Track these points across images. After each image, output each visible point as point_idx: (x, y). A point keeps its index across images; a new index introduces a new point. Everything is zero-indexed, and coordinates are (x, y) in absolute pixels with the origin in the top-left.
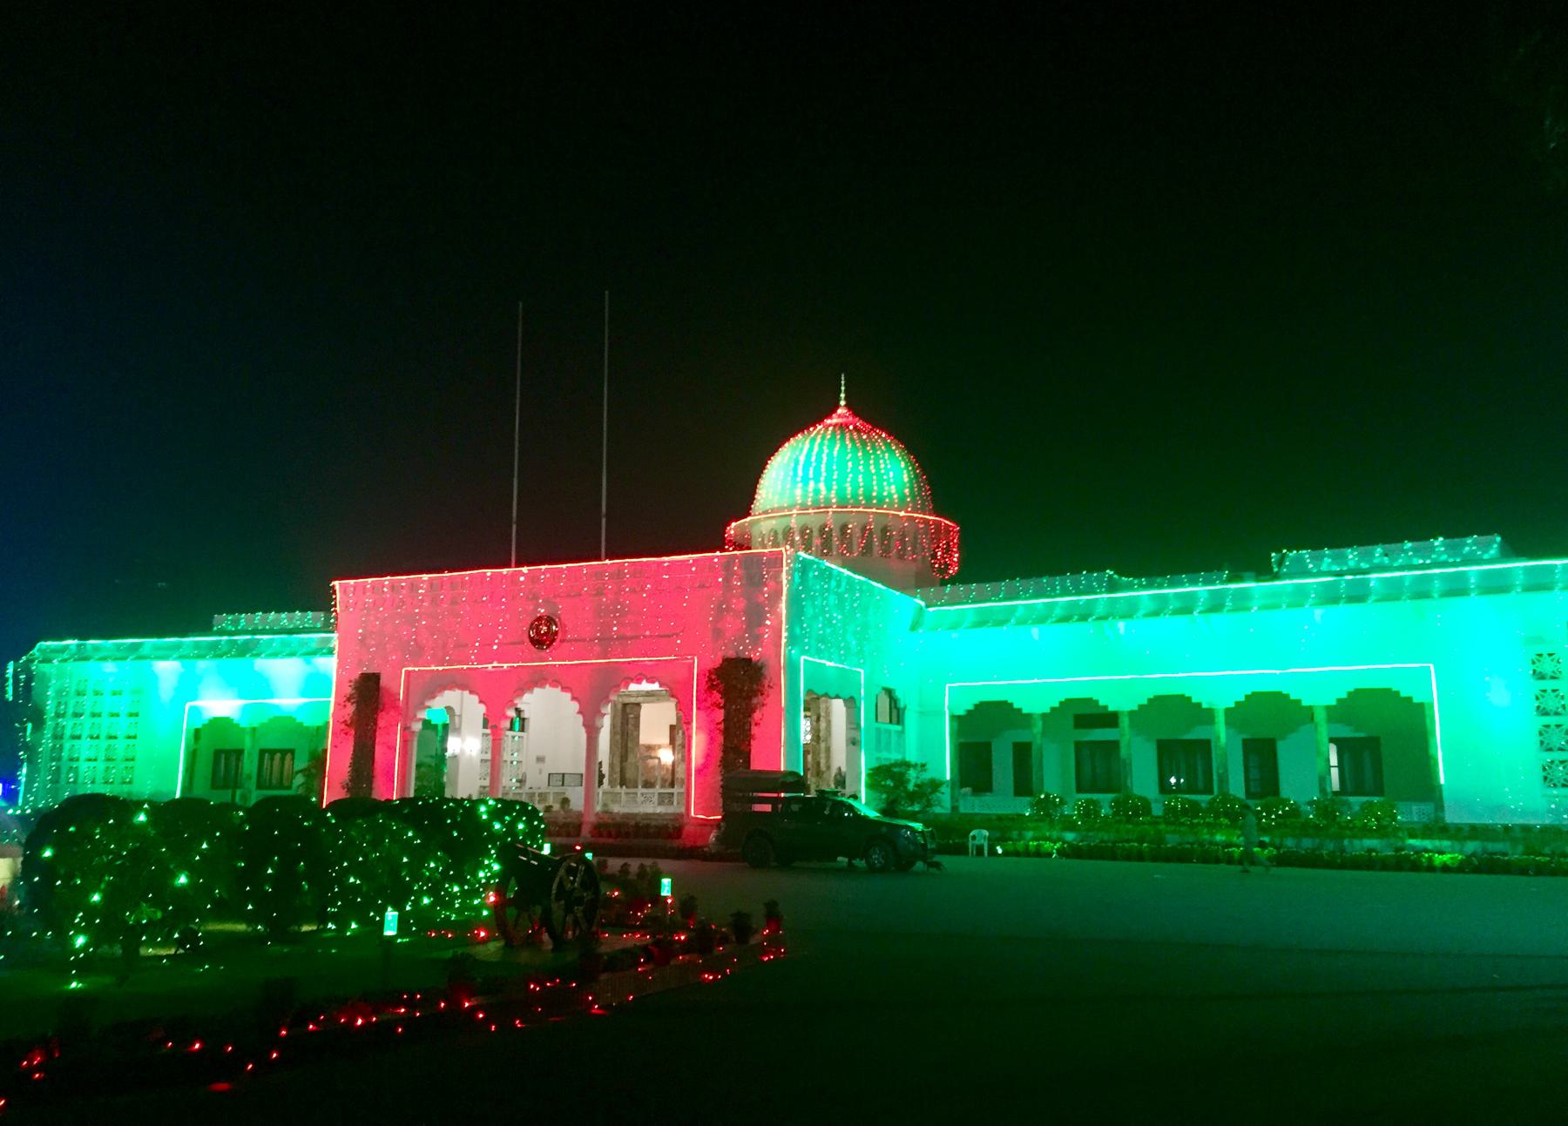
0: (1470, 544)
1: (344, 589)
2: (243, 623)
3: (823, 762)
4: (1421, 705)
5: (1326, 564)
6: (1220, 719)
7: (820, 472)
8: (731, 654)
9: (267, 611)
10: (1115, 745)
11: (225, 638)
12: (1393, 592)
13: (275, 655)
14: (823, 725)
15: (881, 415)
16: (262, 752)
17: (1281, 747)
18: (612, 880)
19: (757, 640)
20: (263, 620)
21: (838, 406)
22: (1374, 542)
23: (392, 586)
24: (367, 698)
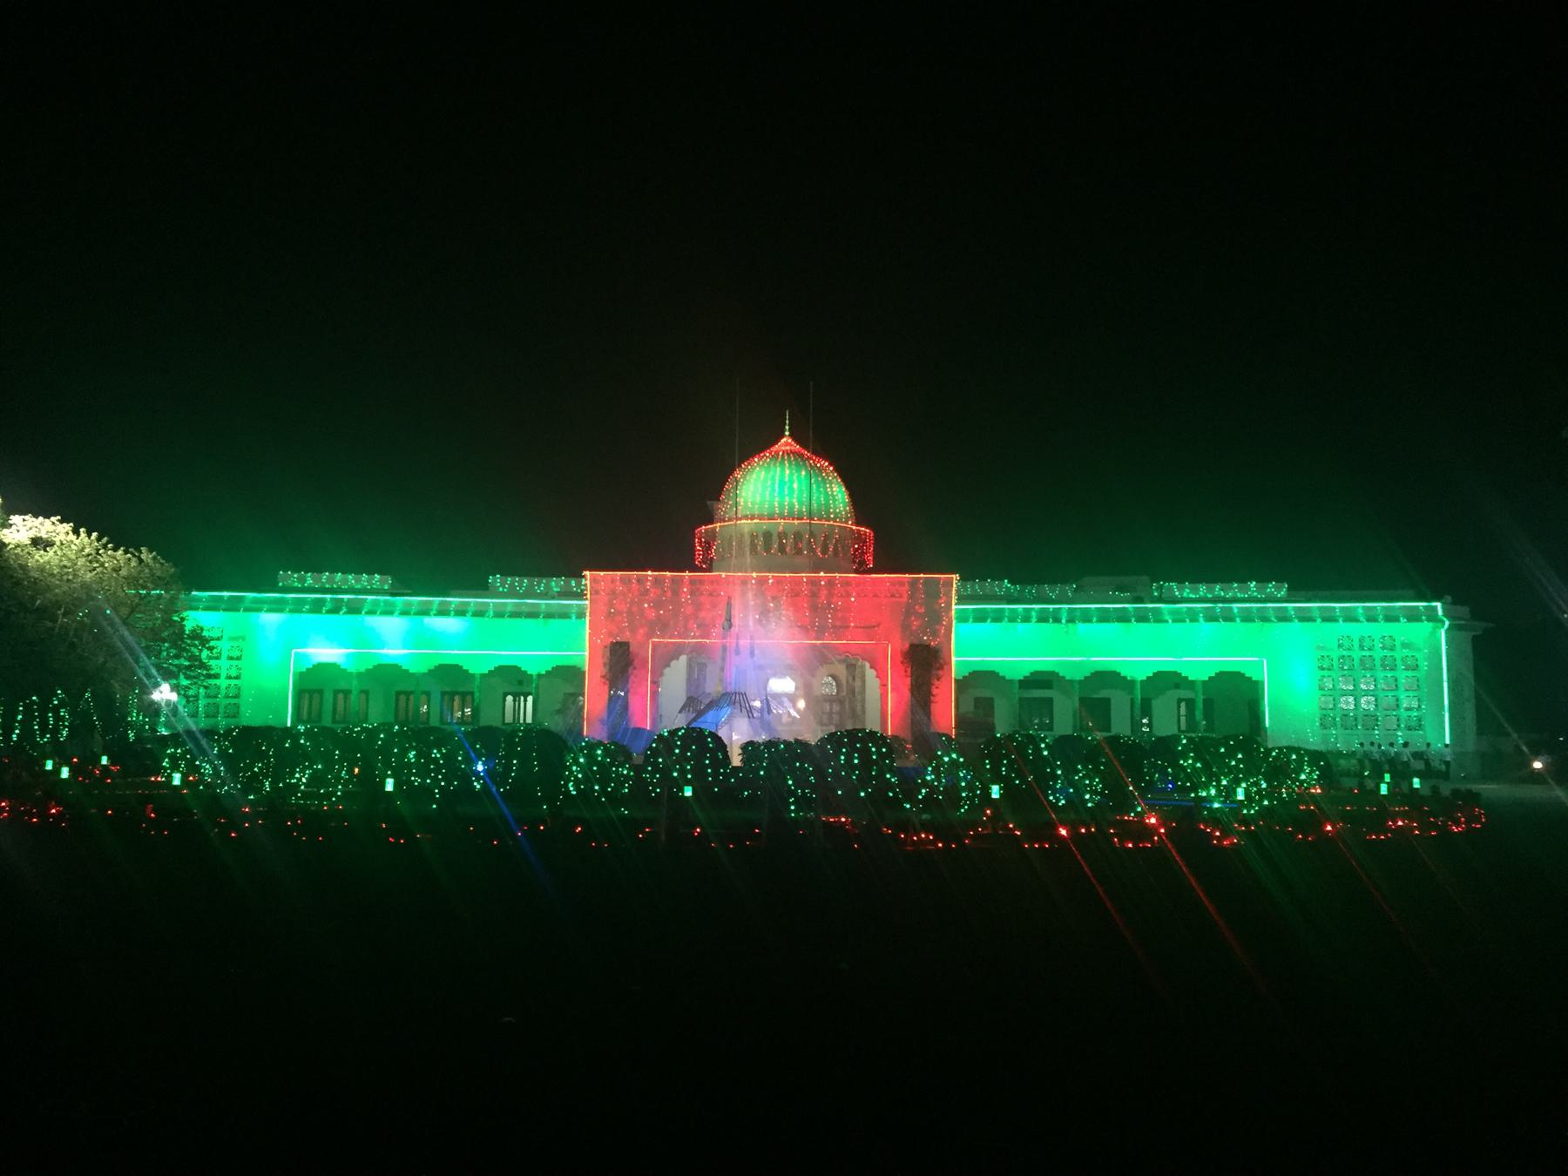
0: (1271, 587)
1: (593, 580)
2: (309, 581)
3: (859, 708)
4: (1256, 683)
5: (1187, 593)
6: (1139, 686)
7: (777, 488)
8: (916, 641)
9: (333, 571)
10: (1050, 700)
11: (328, 596)
12: (1247, 617)
13: (371, 612)
14: (858, 683)
15: (825, 443)
16: (398, 694)
17: (1154, 702)
18: (449, 783)
19: (935, 634)
20: (330, 580)
21: (783, 436)
22: (1215, 581)
23: (656, 581)
24: (620, 661)
